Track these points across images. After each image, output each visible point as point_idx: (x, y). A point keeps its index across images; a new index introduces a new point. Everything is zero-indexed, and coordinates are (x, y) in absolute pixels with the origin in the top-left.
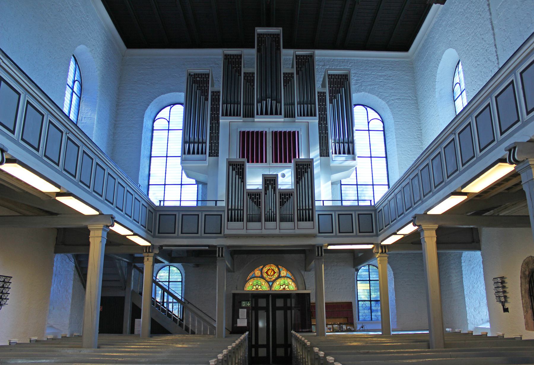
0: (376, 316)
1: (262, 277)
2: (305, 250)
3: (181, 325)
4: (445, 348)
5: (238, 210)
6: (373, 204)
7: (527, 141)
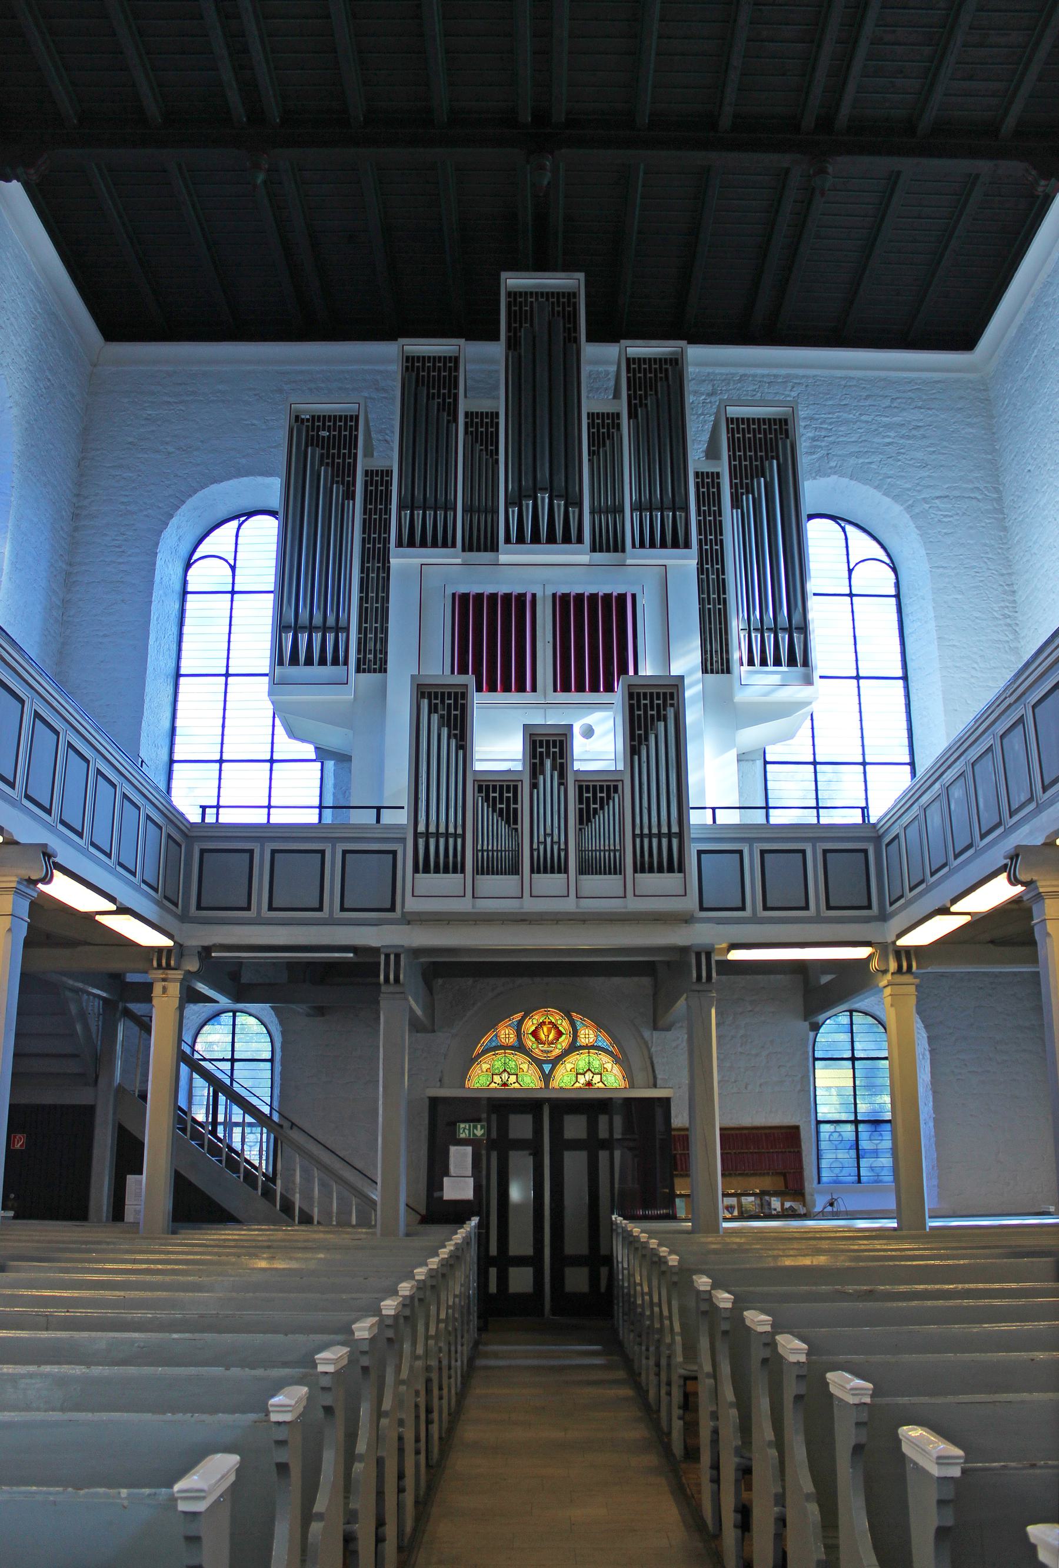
1: (520, 1048)
2: (652, 964)
3: (268, 1194)
5: (447, 835)
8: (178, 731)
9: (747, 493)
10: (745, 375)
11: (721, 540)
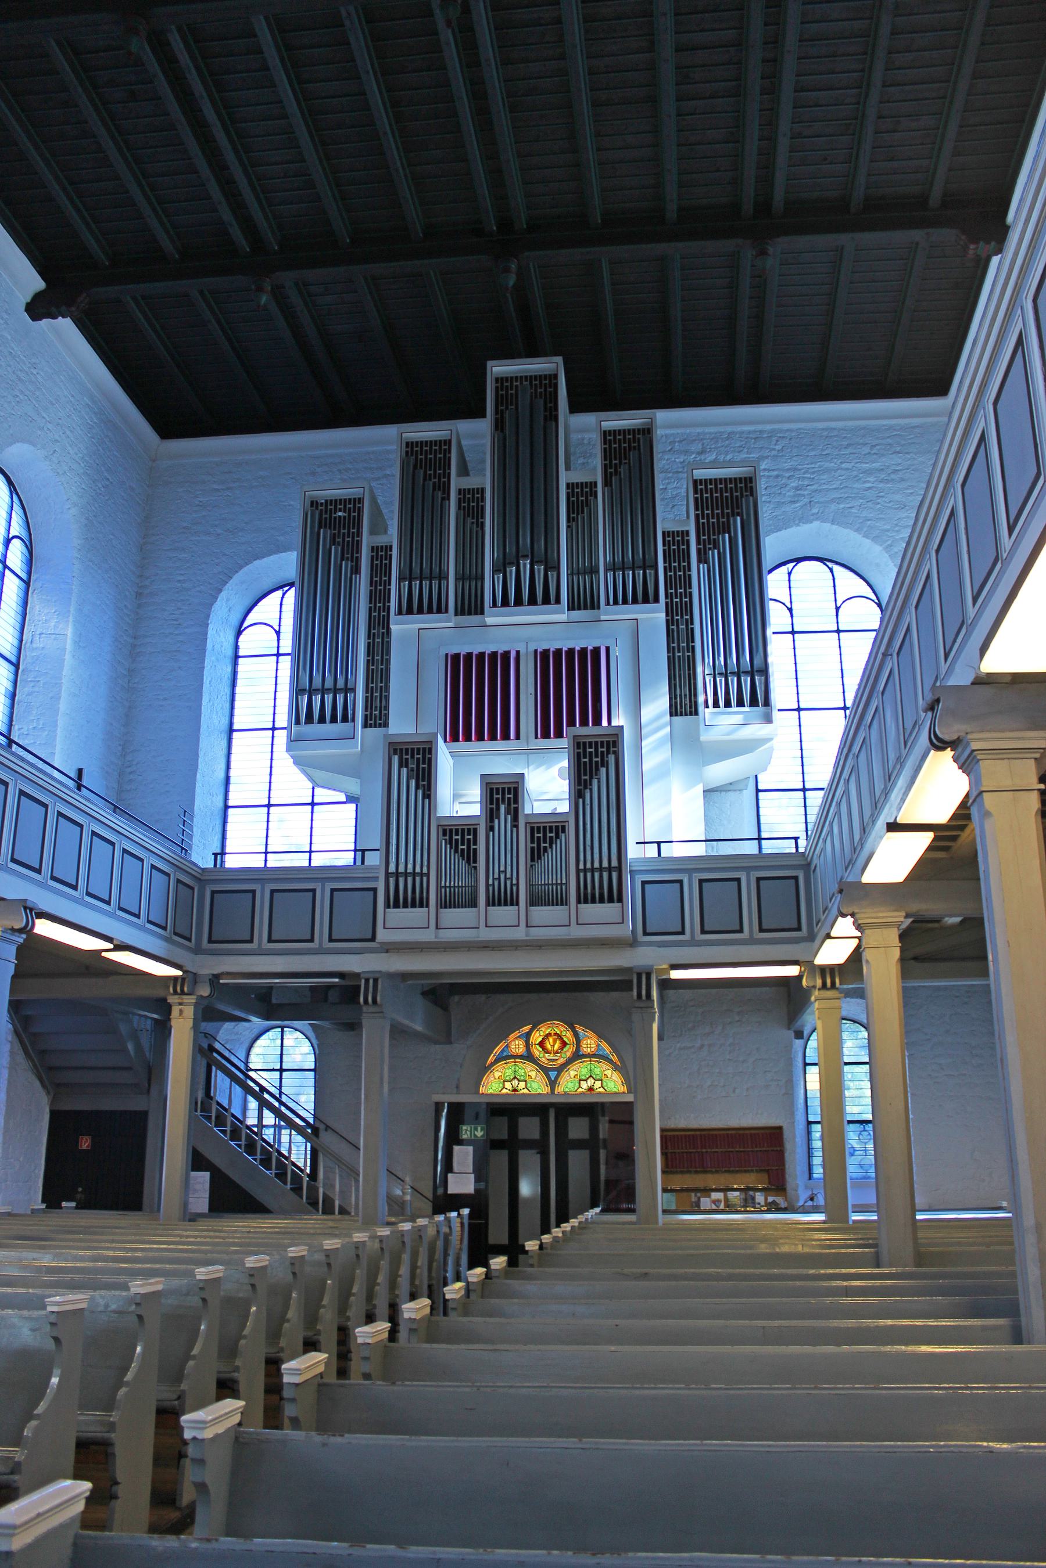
0: (861, 1165)
1: (529, 1057)
7: (972, 684)
8: (232, 780)
10: (733, 433)
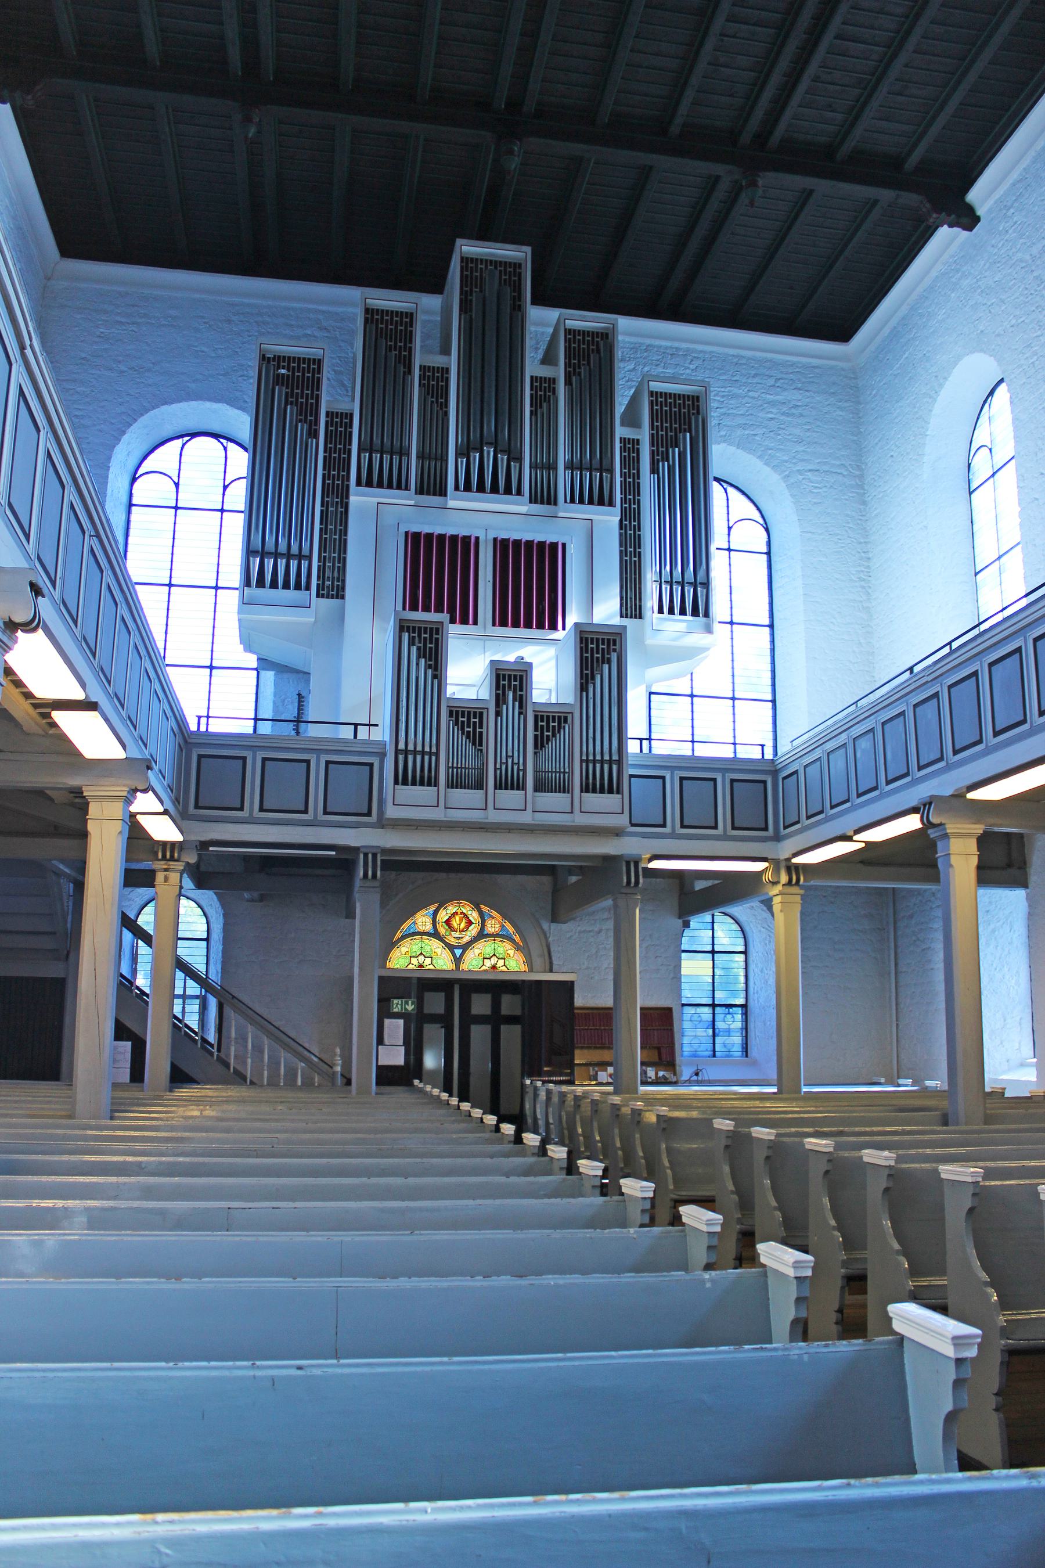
0: (724, 1044)
1: (436, 935)
4: (985, 1124)
6: (769, 755)
9: (663, 461)
11: (639, 501)
